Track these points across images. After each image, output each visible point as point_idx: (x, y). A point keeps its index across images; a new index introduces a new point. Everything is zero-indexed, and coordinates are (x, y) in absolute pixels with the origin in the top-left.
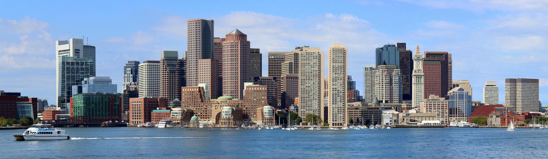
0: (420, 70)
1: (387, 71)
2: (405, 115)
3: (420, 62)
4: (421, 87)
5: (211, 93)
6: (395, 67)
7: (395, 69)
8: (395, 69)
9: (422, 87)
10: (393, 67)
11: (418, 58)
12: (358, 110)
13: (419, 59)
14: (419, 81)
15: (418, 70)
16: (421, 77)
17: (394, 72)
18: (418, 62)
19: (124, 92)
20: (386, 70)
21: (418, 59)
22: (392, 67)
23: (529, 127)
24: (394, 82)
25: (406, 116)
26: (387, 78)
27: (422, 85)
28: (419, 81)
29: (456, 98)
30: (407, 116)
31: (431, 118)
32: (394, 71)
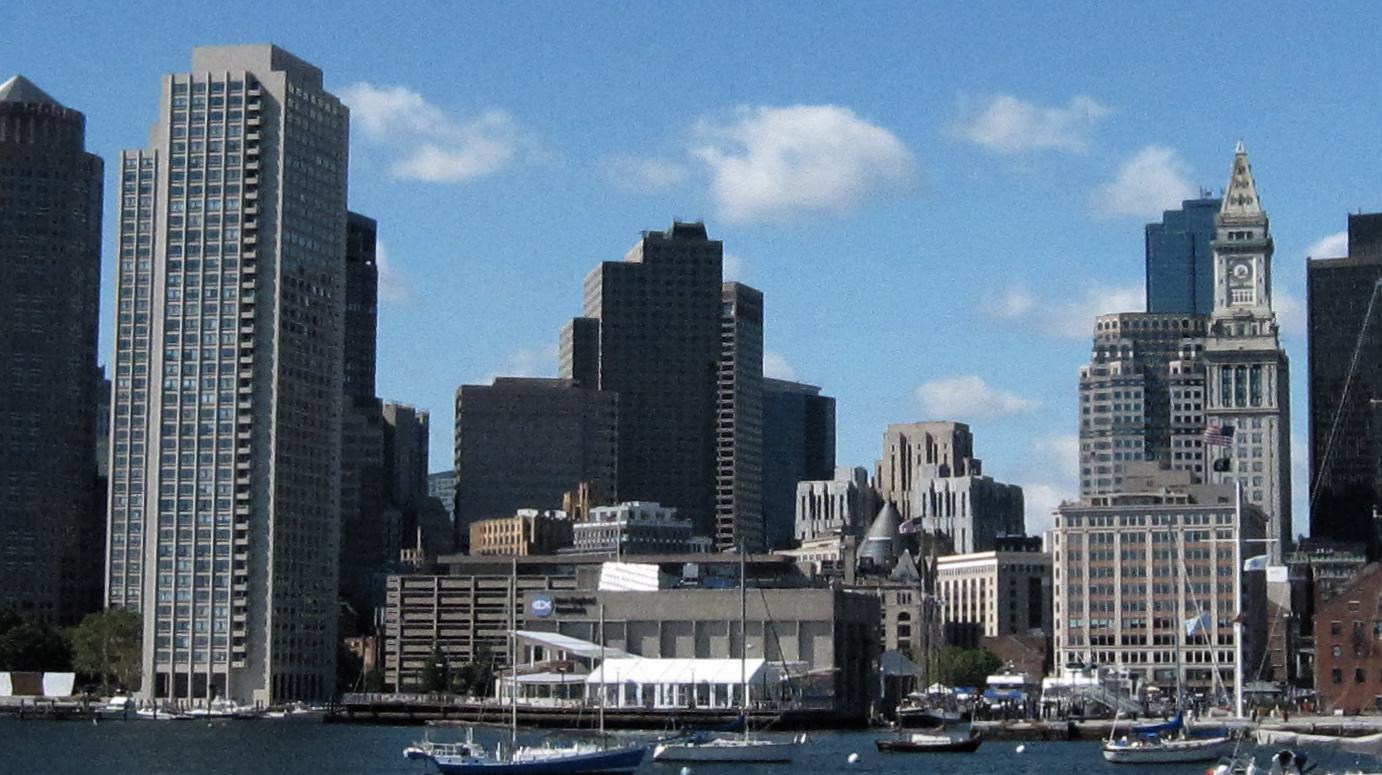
0: (1251, 318)
1: (1131, 354)
2: (548, 605)
3: (1254, 262)
4: (1256, 439)
5: (496, 518)
6: (1185, 324)
7: (1187, 341)
8: (1186, 336)
9: (1265, 437)
10: (1160, 328)
11: (1240, 235)
12: (469, 584)
13: (1245, 241)
14: (1240, 395)
15: (1238, 319)
16: (1258, 367)
17: (1177, 358)
18: (1239, 261)
19: (1230, 518)
20: (1125, 349)
21: (1234, 241)
22: (1165, 324)
23: (184, 716)
24: (1178, 419)
25: (559, 619)
26: (1187, 395)
27: (1265, 422)
28: (1240, 395)
29: (1117, 491)
30: (568, 618)
31: (720, 642)
32: (1181, 354)
